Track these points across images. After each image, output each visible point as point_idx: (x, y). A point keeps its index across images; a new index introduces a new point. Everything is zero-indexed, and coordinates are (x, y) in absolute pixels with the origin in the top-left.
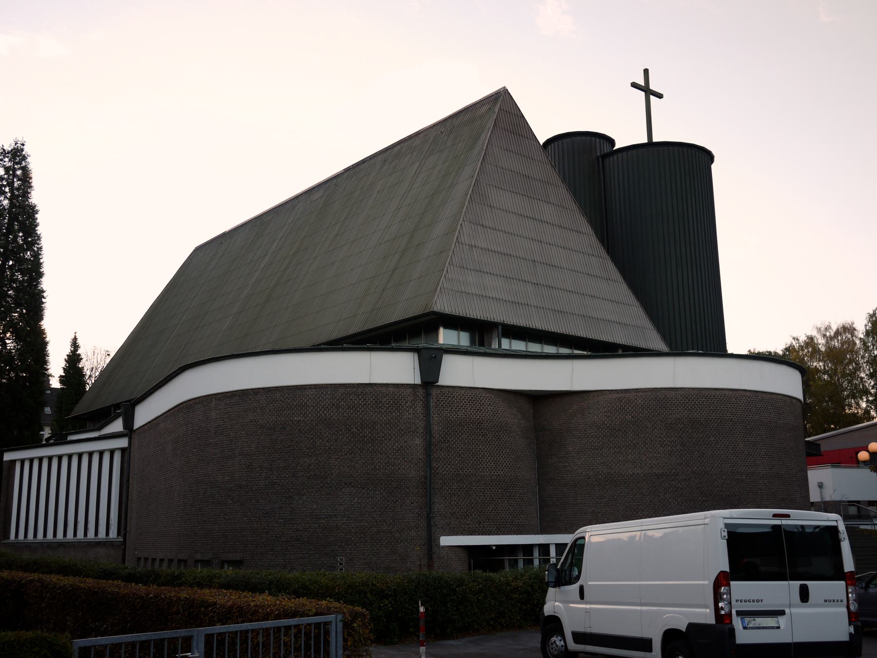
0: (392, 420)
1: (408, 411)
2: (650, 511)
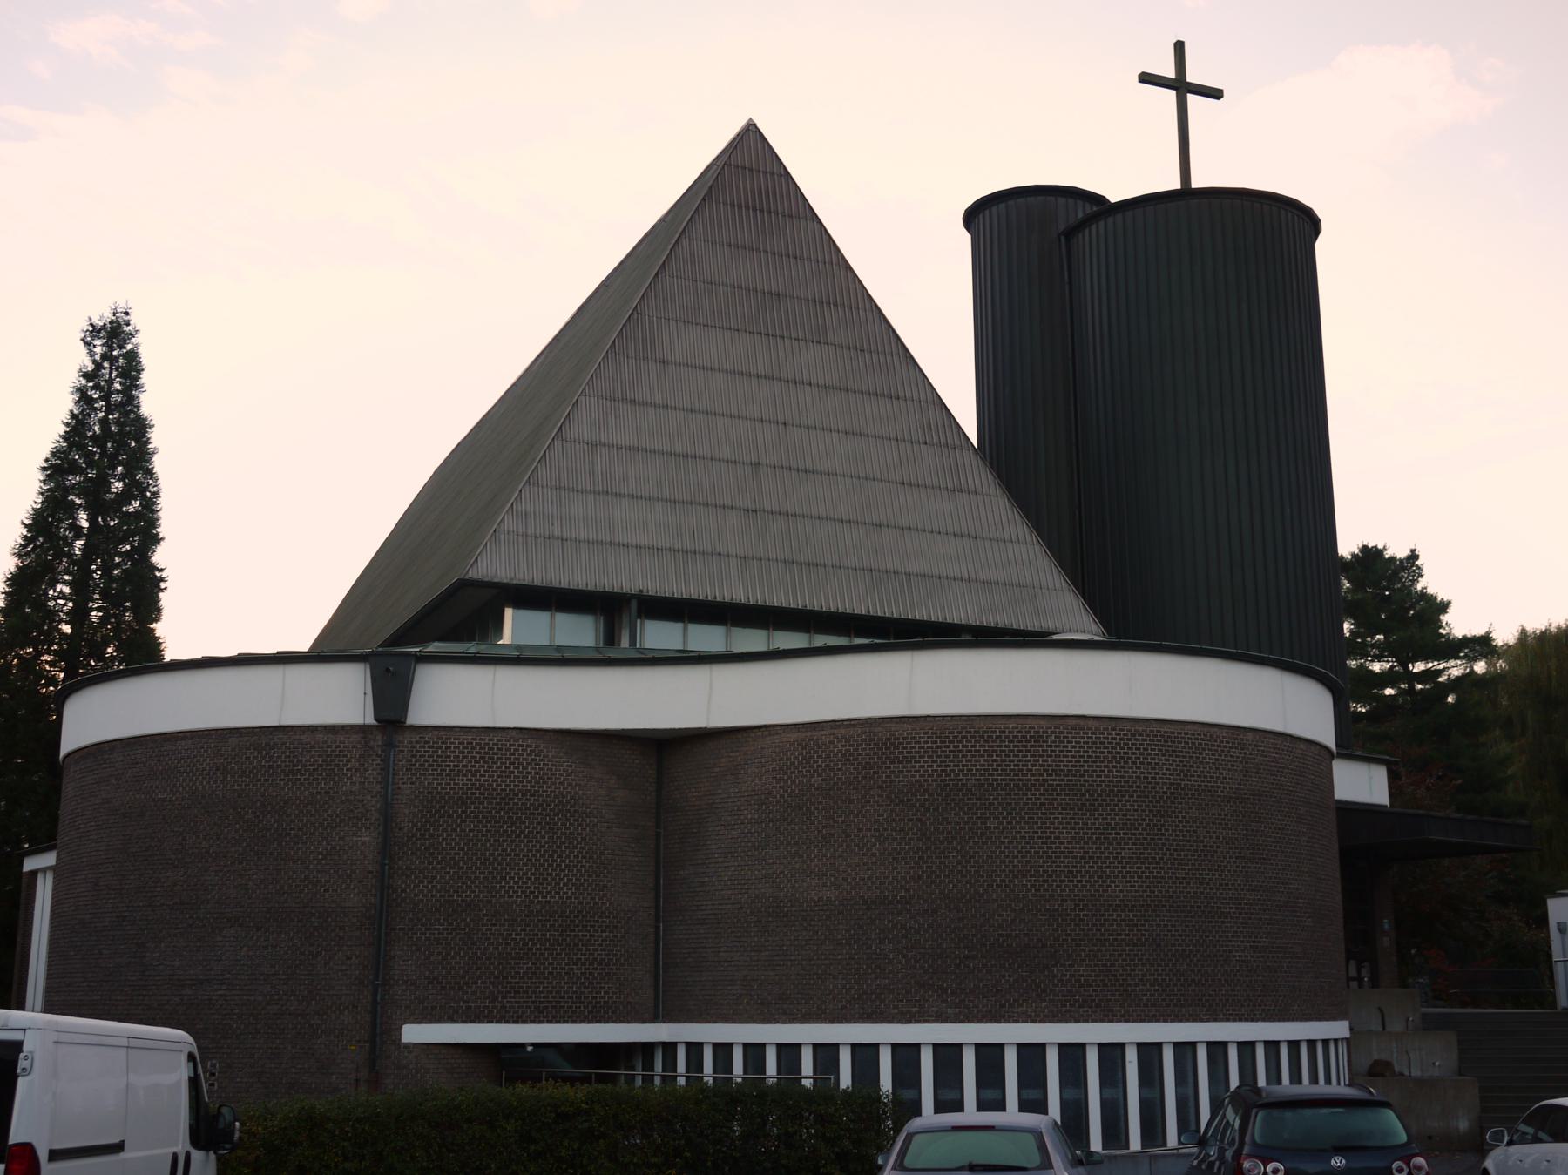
0: (319, 797)
1: (351, 779)
2: (849, 977)
